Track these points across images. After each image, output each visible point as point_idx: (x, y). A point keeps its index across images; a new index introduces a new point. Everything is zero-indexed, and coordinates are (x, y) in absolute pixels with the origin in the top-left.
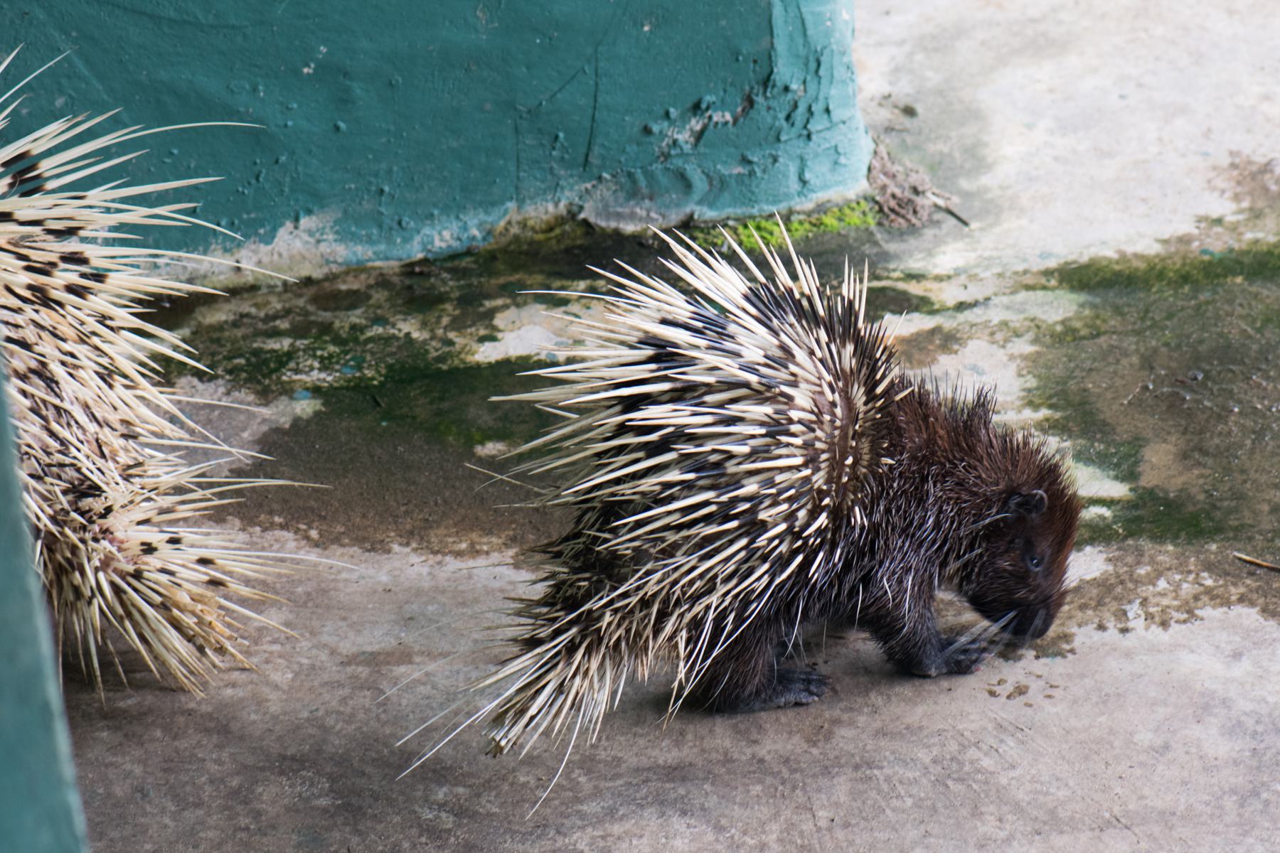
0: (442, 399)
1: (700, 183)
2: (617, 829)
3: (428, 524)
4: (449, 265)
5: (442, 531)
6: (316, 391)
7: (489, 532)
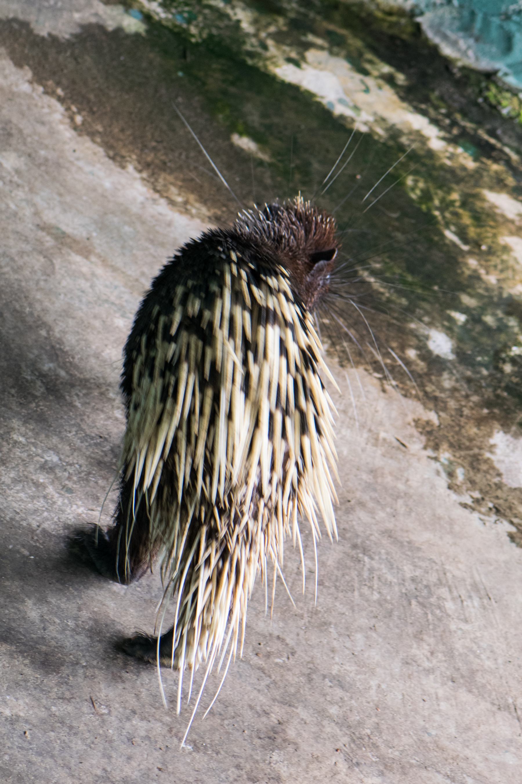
0: (233, 83)
3: (163, 167)
7: (204, 201)
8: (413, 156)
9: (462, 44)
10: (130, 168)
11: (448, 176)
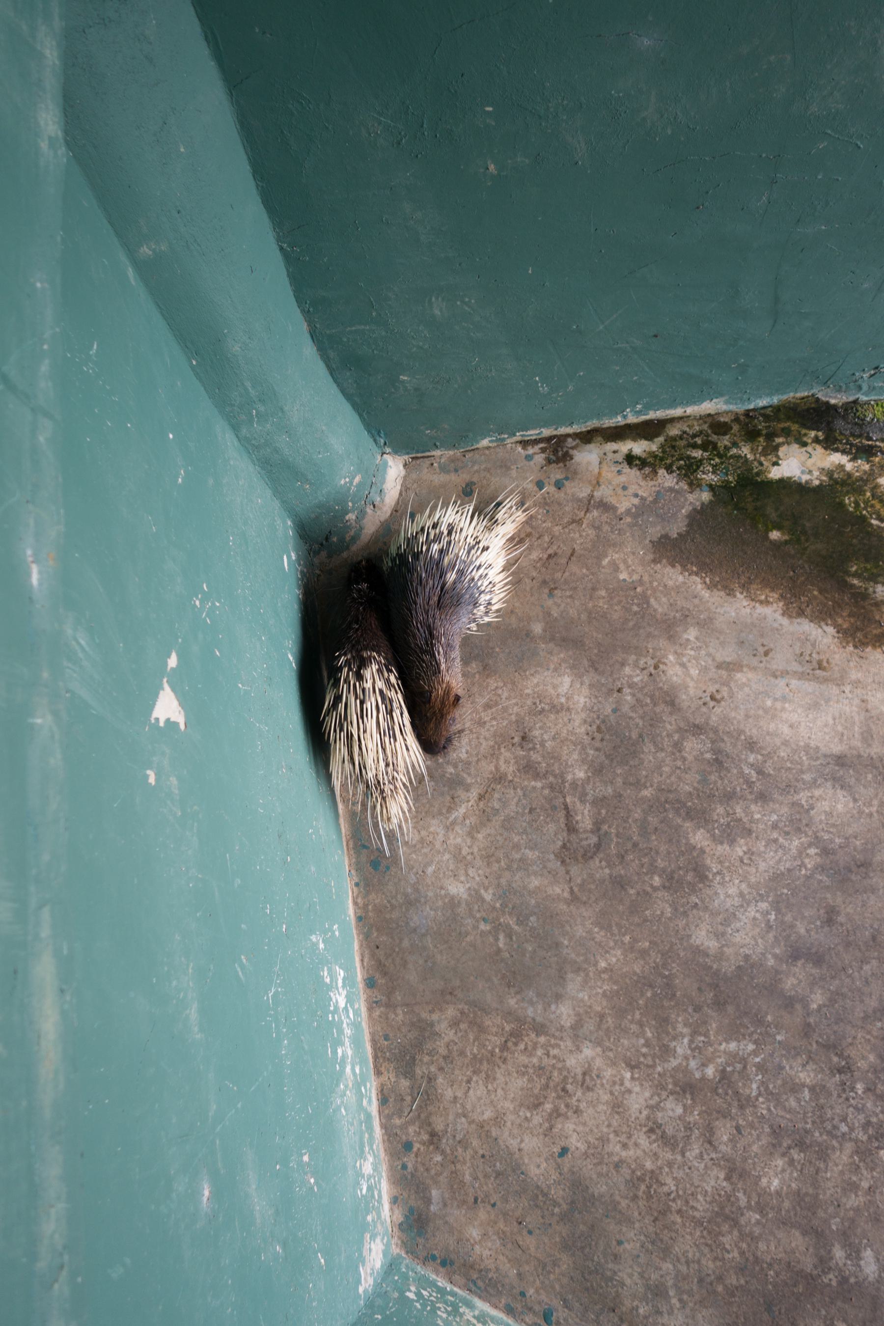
0: (757, 499)
1: (865, 387)
2: (817, 793)
3: (750, 582)
4: (762, 411)
5: (755, 586)
6: (711, 488)
7: (773, 590)
8: (843, 483)
9: (839, 396)
10: (738, 595)
11: (861, 483)
